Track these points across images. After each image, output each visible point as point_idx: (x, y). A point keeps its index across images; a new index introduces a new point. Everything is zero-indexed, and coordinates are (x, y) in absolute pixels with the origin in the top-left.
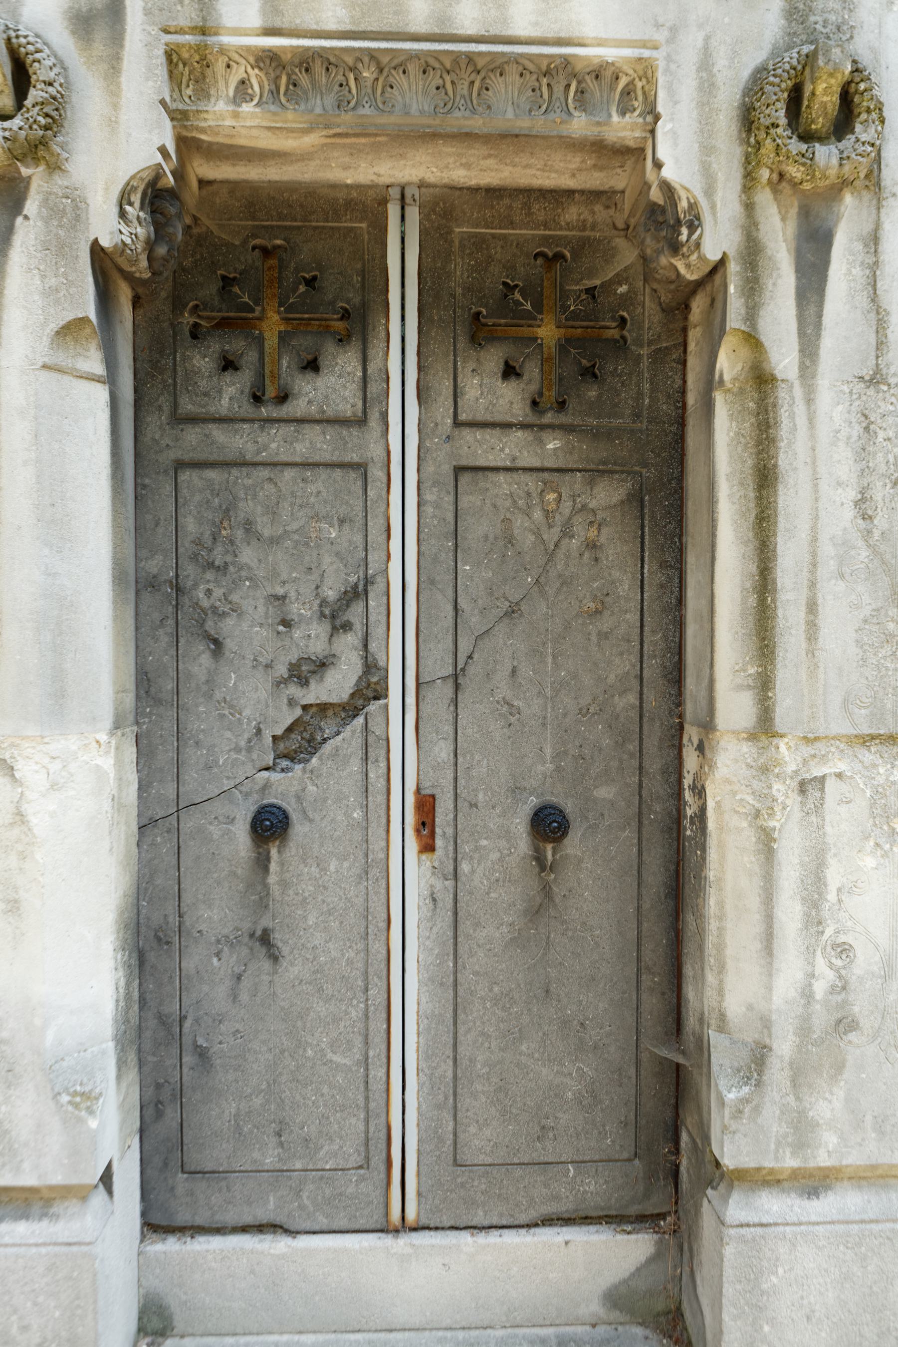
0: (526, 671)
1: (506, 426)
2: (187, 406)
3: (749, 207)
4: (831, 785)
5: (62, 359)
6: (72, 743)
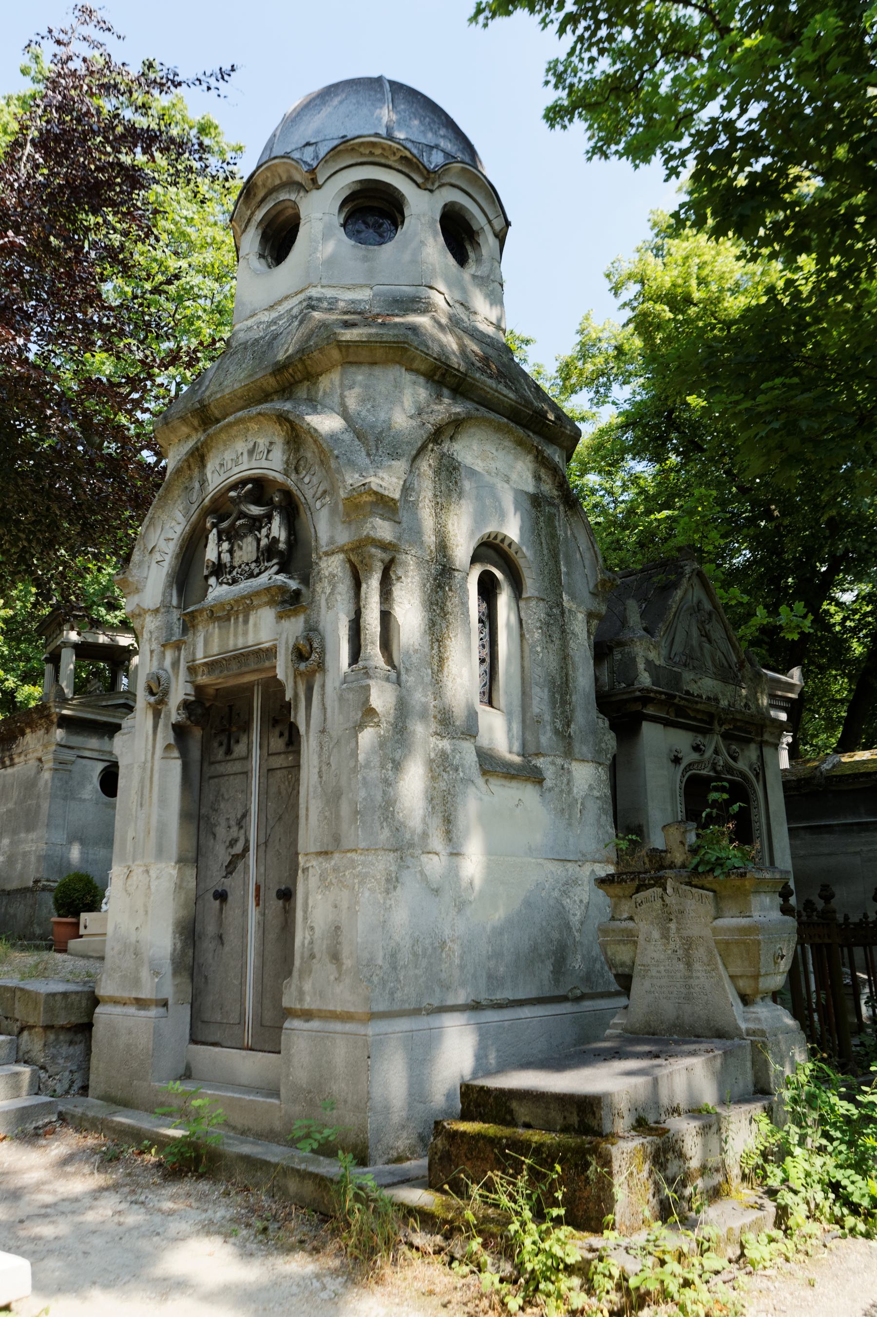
0: (283, 840)
1: (279, 754)
2: (212, 759)
3: (295, 683)
4: (311, 870)
5: (167, 755)
6: (163, 865)
